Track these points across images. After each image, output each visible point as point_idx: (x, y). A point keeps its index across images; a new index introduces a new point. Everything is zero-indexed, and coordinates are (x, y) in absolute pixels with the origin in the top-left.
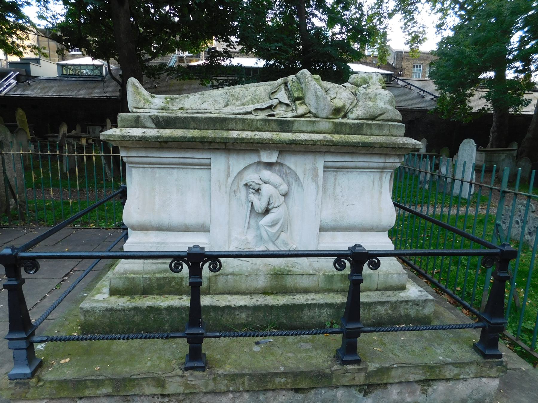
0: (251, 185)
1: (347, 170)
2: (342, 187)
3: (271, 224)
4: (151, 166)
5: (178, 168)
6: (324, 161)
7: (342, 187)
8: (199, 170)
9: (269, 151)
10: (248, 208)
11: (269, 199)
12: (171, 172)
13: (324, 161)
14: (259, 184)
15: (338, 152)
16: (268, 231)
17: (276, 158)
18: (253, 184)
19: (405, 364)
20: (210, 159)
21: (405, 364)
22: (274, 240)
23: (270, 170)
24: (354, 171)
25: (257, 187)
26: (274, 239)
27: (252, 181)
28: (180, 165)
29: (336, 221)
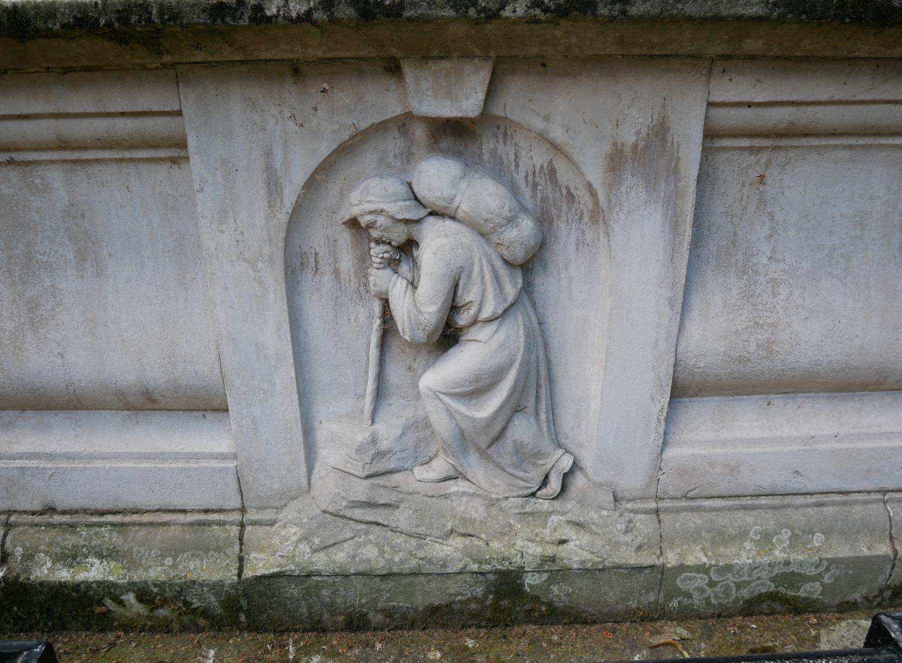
0: (371, 225)
1: (804, 142)
2: (772, 220)
3: (466, 389)
4: (117, 155)
5: (65, 161)
6: (710, 105)
7: (772, 220)
8: (153, 167)
9: (445, 64)
10: (371, 317)
11: (456, 287)
12: (38, 181)
13: (710, 105)
14: (407, 222)
15: (553, 414)
16: (457, 411)
17: (481, 96)
18: (381, 220)
19: (840, 493)
20: (179, 113)
21: (840, 493)
22: (483, 446)
23: (456, 155)
24: (836, 147)
25: (398, 235)
26: (483, 442)
27: (372, 207)
28: (111, 148)
29: (741, 360)
